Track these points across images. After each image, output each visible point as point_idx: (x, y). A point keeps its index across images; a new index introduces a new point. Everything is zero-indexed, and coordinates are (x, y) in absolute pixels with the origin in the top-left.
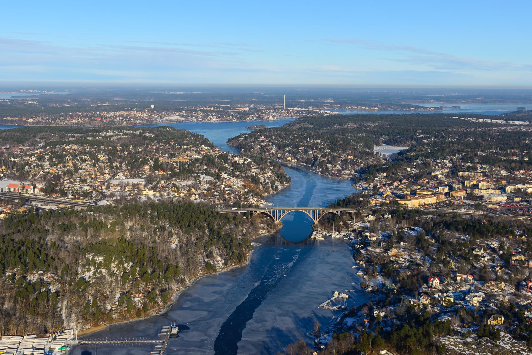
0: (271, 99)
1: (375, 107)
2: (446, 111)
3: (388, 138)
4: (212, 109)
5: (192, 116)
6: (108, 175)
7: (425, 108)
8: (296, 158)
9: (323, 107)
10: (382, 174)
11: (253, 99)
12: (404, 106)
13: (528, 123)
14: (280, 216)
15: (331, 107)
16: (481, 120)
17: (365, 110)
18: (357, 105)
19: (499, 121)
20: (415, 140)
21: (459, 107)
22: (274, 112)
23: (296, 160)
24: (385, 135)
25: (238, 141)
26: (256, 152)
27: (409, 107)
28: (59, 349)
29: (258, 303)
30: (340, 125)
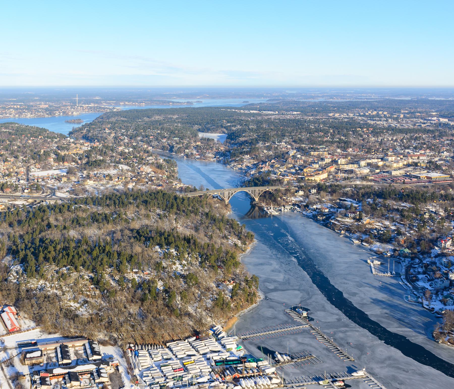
0: (86, 97)
1: (143, 103)
2: (196, 105)
3: (200, 127)
4: (19, 107)
5: (6, 114)
6: (22, 168)
7: (180, 103)
8: (151, 146)
9: (102, 104)
10: (246, 156)
11: (35, 98)
12: (164, 102)
13: (277, 112)
14: (229, 197)
15: (109, 103)
16: (242, 111)
17: (135, 105)
18: (129, 101)
19: (255, 112)
20: (225, 128)
21: (201, 102)
22: (71, 108)
23: (151, 148)
24: (197, 124)
25: (82, 133)
26: (110, 142)
27: (169, 102)
28: (236, 348)
29: (326, 281)
30: (148, 117)
